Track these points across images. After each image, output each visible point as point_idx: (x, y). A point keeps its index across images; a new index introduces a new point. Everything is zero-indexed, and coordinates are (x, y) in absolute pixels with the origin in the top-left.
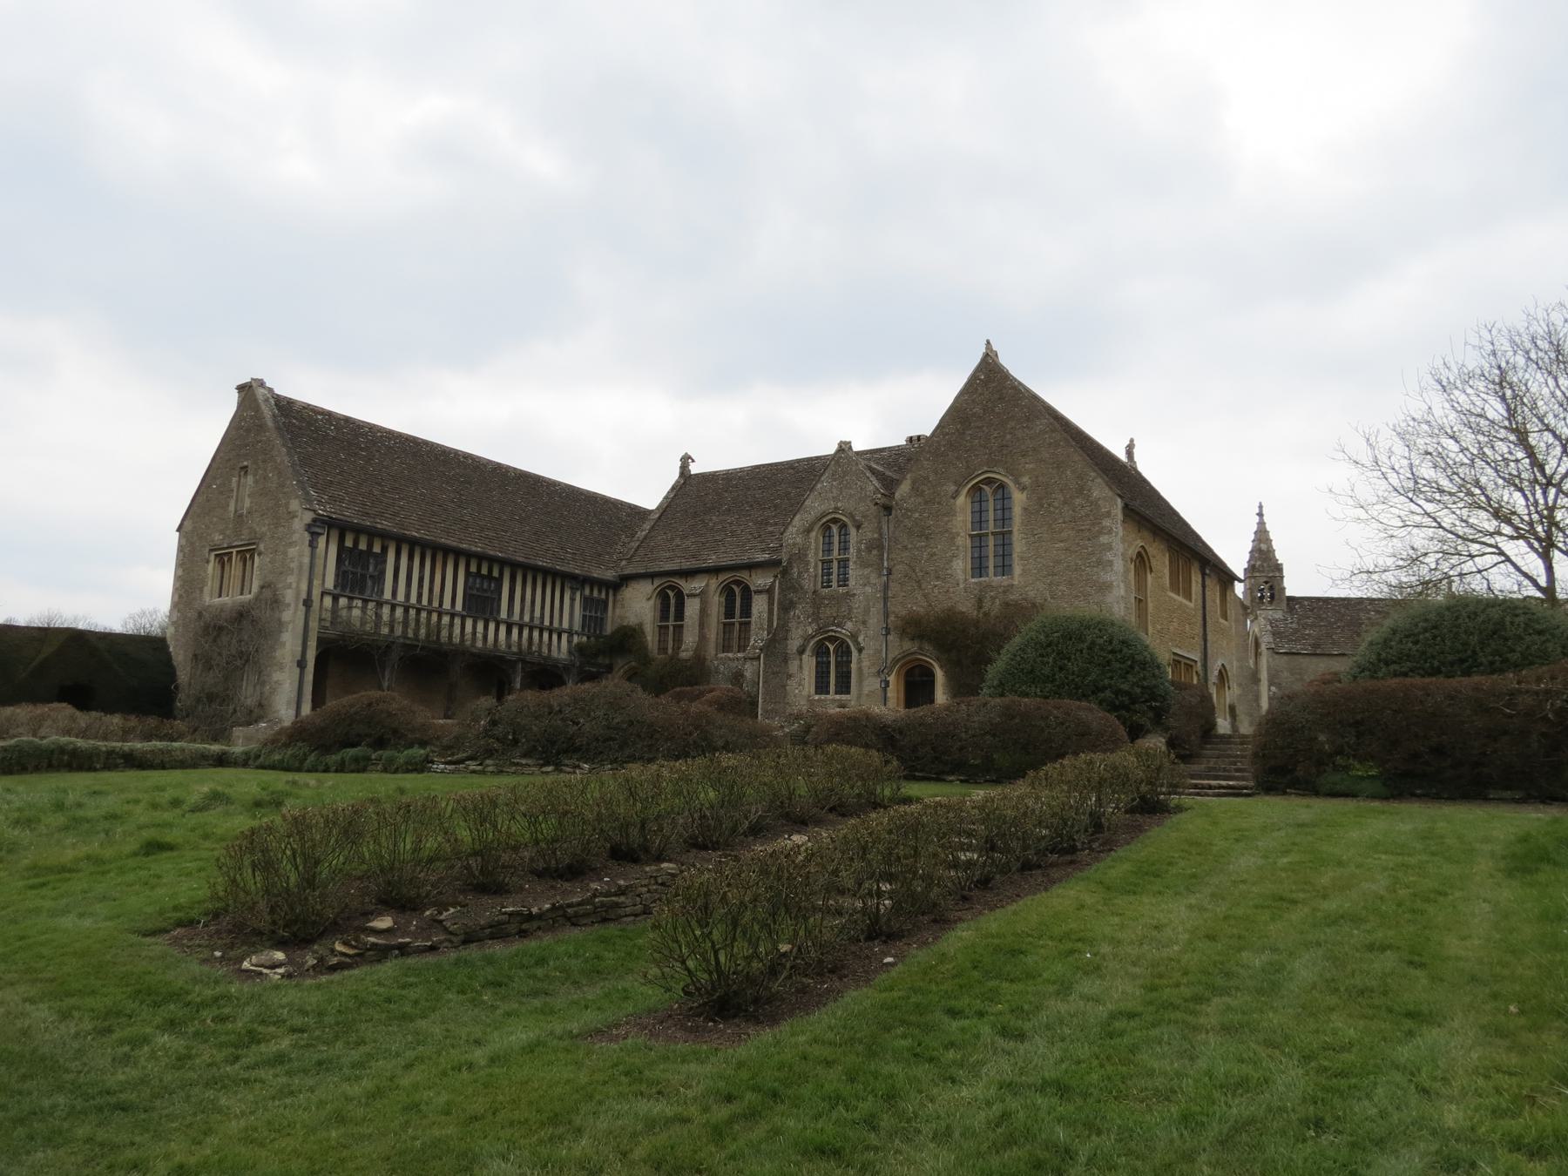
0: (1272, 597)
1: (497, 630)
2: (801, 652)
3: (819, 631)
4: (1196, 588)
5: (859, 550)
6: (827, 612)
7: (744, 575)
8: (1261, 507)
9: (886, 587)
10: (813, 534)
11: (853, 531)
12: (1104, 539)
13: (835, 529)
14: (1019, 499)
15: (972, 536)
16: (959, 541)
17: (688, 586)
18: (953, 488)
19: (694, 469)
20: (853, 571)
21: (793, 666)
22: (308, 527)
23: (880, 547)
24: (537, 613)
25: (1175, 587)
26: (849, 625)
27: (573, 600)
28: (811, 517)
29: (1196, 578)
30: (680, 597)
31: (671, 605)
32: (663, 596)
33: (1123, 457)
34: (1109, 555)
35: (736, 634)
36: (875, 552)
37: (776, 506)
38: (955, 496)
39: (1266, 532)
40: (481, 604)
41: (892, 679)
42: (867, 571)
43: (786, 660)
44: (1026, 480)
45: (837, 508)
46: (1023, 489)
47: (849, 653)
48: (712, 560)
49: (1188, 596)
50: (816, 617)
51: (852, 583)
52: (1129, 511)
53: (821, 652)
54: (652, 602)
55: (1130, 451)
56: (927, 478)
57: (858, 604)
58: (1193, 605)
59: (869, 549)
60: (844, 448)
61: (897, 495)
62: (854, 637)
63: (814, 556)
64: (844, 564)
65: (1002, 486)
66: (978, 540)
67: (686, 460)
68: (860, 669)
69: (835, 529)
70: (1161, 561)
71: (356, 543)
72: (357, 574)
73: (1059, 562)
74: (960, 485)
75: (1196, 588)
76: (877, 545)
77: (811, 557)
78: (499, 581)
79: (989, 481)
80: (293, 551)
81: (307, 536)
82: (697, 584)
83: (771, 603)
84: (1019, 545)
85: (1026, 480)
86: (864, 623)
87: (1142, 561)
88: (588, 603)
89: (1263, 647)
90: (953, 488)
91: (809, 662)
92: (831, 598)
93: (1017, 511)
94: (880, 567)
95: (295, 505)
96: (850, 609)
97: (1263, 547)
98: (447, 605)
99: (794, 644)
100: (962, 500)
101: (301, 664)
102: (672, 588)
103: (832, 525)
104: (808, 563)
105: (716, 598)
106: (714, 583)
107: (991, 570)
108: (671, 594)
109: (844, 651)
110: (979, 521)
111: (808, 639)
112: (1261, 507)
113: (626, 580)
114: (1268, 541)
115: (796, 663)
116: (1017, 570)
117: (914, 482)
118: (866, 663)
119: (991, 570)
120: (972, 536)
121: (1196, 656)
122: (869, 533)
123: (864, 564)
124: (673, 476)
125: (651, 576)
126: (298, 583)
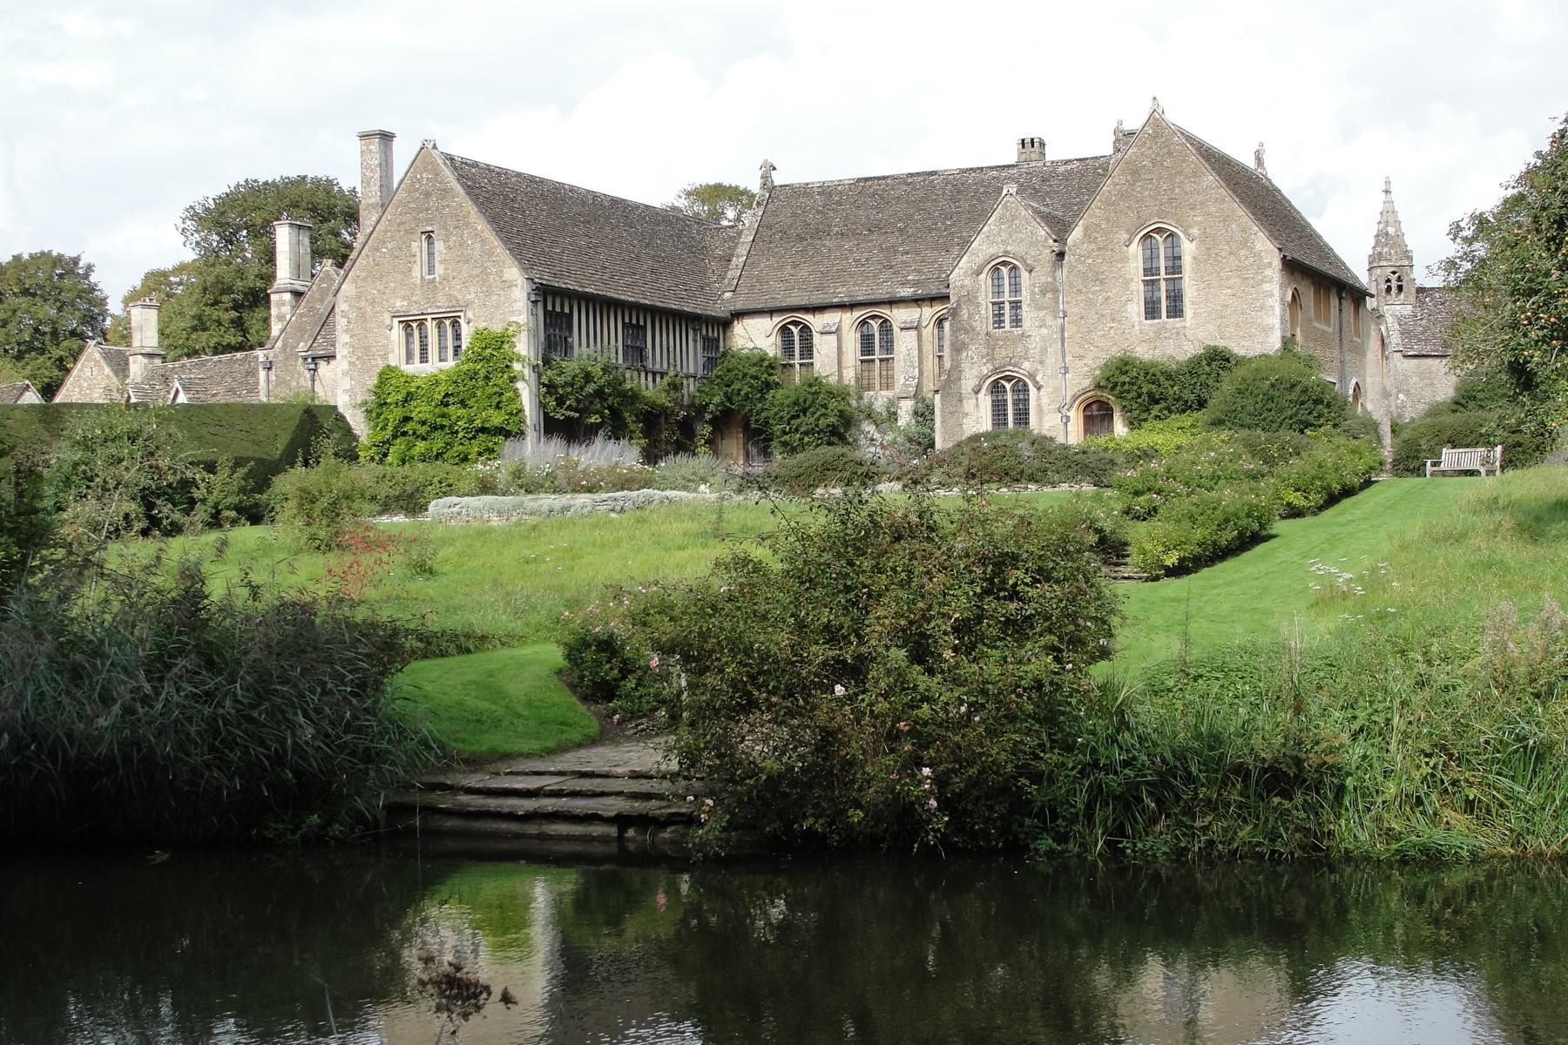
0: (1400, 288)
2: (977, 392)
3: (995, 371)
5: (1033, 293)
6: (1001, 354)
7: (885, 311)
8: (1388, 183)
10: (983, 276)
11: (1024, 275)
12: (1266, 287)
14: (1188, 249)
16: (1133, 286)
17: (816, 322)
18: (1126, 236)
19: (778, 179)
20: (1026, 313)
21: (968, 405)
23: (1055, 291)
25: (1318, 317)
26: (1026, 365)
27: (695, 341)
28: (980, 260)
29: (1334, 302)
31: (797, 340)
32: (784, 330)
33: (1251, 163)
36: (1049, 295)
37: (900, 230)
40: (636, 352)
42: (1042, 314)
44: (1195, 231)
47: (1026, 390)
48: (842, 296)
49: (1327, 322)
51: (1026, 324)
52: (1291, 267)
53: (996, 388)
55: (1259, 160)
56: (1099, 225)
57: (1034, 345)
59: (1043, 292)
62: (1032, 376)
63: (985, 298)
64: (1016, 306)
68: (1039, 406)
70: (1308, 295)
73: (1226, 306)
75: (1334, 311)
76: (1052, 289)
77: (981, 299)
79: (1159, 231)
85: (1195, 231)
88: (711, 344)
90: (1126, 236)
91: (986, 400)
93: (1187, 262)
94: (1055, 312)
96: (1027, 350)
97: (1391, 230)
99: (968, 384)
100: (1135, 248)
102: (795, 323)
105: (852, 334)
106: (848, 319)
108: (795, 330)
109: (1021, 388)
112: (1388, 183)
117: (1086, 229)
118: (1045, 401)
125: (771, 312)
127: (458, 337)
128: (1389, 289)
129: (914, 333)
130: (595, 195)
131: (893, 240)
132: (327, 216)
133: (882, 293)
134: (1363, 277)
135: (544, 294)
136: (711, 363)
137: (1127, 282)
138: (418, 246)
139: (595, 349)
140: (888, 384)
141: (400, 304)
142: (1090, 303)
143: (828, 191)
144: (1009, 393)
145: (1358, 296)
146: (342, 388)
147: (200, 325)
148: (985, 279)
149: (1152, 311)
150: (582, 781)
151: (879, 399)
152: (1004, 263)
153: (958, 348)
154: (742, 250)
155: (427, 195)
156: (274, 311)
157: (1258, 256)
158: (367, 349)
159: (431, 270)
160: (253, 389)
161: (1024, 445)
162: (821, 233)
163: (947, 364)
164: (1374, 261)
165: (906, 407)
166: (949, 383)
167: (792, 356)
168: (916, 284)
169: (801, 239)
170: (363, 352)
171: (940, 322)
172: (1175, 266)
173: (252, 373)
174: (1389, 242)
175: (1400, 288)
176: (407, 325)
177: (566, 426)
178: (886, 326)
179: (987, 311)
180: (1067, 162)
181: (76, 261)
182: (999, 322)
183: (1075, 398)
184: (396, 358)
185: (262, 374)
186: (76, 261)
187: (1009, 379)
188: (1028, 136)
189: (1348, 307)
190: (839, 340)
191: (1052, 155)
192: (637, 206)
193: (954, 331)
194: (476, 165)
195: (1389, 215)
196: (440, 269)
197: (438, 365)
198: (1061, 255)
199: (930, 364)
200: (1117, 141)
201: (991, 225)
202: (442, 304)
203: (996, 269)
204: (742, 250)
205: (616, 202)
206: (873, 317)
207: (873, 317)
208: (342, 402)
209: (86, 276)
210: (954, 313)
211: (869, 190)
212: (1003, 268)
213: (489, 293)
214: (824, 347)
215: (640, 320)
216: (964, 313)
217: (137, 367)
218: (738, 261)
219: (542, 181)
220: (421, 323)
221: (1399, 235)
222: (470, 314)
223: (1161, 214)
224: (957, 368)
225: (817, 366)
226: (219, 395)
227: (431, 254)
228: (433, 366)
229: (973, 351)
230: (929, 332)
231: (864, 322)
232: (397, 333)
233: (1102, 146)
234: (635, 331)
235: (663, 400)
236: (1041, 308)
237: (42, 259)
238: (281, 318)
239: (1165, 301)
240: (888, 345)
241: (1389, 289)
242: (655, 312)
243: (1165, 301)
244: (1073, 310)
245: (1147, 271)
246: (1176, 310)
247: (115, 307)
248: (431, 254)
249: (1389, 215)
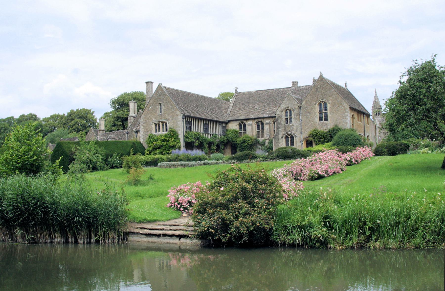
0: (379, 114)
2: (282, 138)
4: (362, 119)
7: (262, 120)
9: (301, 124)
11: (292, 112)
12: (346, 114)
13: (288, 111)
14: (329, 106)
17: (247, 123)
18: (315, 103)
19: (239, 91)
21: (280, 141)
25: (358, 120)
26: (293, 132)
28: (283, 108)
29: (362, 117)
32: (240, 125)
33: (344, 86)
34: (347, 117)
39: (377, 97)
40: (206, 131)
41: (303, 143)
44: (330, 101)
46: (329, 104)
47: (293, 137)
48: (253, 117)
49: (361, 122)
50: (285, 131)
51: (293, 123)
52: (352, 109)
53: (287, 137)
55: (346, 85)
57: (295, 127)
58: (362, 123)
59: (297, 116)
61: (302, 104)
62: (294, 134)
63: (284, 117)
64: (291, 119)
67: (236, 89)
68: (296, 141)
69: (288, 111)
70: (356, 116)
73: (337, 118)
74: (316, 102)
75: (362, 119)
76: (299, 115)
79: (322, 102)
80: (179, 123)
82: (250, 122)
83: (270, 126)
84: (329, 115)
85: (330, 101)
87: (353, 117)
88: (224, 128)
89: (377, 127)
90: (315, 103)
91: (284, 140)
92: (288, 126)
93: (328, 108)
94: (299, 120)
95: (178, 113)
97: (377, 101)
99: (280, 136)
100: (317, 106)
102: (242, 123)
109: (292, 137)
113: (230, 121)
114: (378, 99)
117: (306, 101)
118: (297, 140)
121: (363, 134)
125: (237, 120)
127: (166, 126)
128: (376, 114)
129: (268, 125)
130: (198, 95)
131: (264, 104)
132: (140, 100)
133: (261, 116)
134: (370, 111)
135: (185, 117)
136: (223, 132)
137: (315, 113)
138: (158, 107)
139: (198, 129)
140: (263, 136)
141: (154, 119)
142: (307, 118)
143: (250, 94)
144: (290, 138)
145: (368, 115)
146: (142, 138)
147: (114, 125)
148: (284, 113)
149: (321, 119)
150: (189, 227)
151: (261, 139)
152: (288, 109)
153: (278, 128)
154: (231, 107)
155: (160, 95)
156: (129, 121)
157: (344, 107)
158: (147, 129)
159: (161, 112)
160: (124, 138)
161: (260, 148)
162: (248, 103)
163: (276, 132)
164: (373, 107)
165: (267, 141)
166: (276, 136)
167: (242, 130)
168: (269, 114)
169: (243, 104)
170: (146, 130)
171: (274, 123)
172: (326, 109)
173: (124, 135)
174: (376, 104)
175: (379, 114)
176: (156, 125)
177: (189, 146)
178: (262, 124)
179: (284, 120)
180: (302, 86)
181: (90, 111)
182: (287, 122)
183: (304, 139)
184: (154, 132)
185: (126, 135)
186: (90, 111)
187: (289, 135)
188: (294, 81)
189: (366, 118)
190: (252, 126)
191: (299, 85)
192: (207, 97)
193: (277, 125)
194: (171, 89)
195: (376, 97)
196: (163, 112)
197: (163, 133)
198: (300, 107)
199: (272, 131)
200: (313, 82)
201: (285, 101)
202: (163, 120)
203: (286, 110)
204: (231, 107)
205: (202, 97)
206: (260, 121)
207: (260, 121)
208: (142, 141)
209: (92, 114)
210: (277, 120)
211: (259, 93)
212: (288, 110)
213: (173, 117)
214: (248, 128)
215: (207, 122)
216: (279, 121)
217: (100, 133)
218: (230, 109)
219: (186, 92)
220: (159, 125)
221: (378, 102)
222: (169, 122)
223: (323, 98)
224: (278, 132)
225: (247, 133)
226: (117, 139)
227: (161, 109)
228: (161, 133)
229: (281, 129)
230: (272, 125)
231: (257, 123)
232: (154, 126)
233: (311, 83)
234: (206, 125)
235: (212, 140)
236: (296, 119)
237: (83, 110)
238: (130, 122)
239: (324, 117)
240: (263, 128)
241: (376, 114)
242: (211, 121)
243: (324, 117)
244: (303, 119)
245: (320, 111)
246: (326, 119)
247: (98, 121)
248: (161, 109)
249: (376, 97)
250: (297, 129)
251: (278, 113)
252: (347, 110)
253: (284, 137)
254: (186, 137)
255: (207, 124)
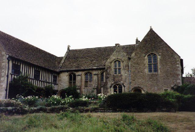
1: (39, 82)
2: (111, 87)
3: (115, 83)
5: (123, 67)
10: (112, 63)
15: (148, 64)
17: (77, 74)
18: (144, 55)
19: (71, 49)
21: (109, 90)
22: (7, 59)
24: (46, 79)
27: (52, 76)
30: (75, 76)
32: (70, 76)
35: (72, 83)
36: (127, 67)
38: (145, 56)
40: (37, 77)
43: (107, 89)
45: (118, 59)
46: (159, 55)
47: (122, 87)
48: (82, 68)
50: (114, 80)
54: (68, 76)
57: (123, 77)
59: (126, 67)
60: (138, 90)
62: (123, 84)
64: (119, 69)
65: (155, 54)
66: (150, 66)
69: (117, 63)
71: (15, 62)
72: (16, 70)
78: (40, 72)
79: (152, 54)
80: (3, 64)
81: (7, 61)
82: (80, 73)
84: (159, 66)
86: (125, 81)
90: (144, 55)
91: (112, 89)
95: (3, 53)
96: (122, 79)
98: (31, 77)
99: (109, 85)
100: (146, 57)
101: (6, 90)
102: (73, 74)
103: (117, 61)
104: (111, 69)
105: (84, 76)
107: (153, 71)
110: (150, 61)
111: (112, 84)
115: (110, 89)
116: (159, 71)
119: (153, 71)
120: (148, 64)
122: (125, 63)
123: (124, 69)
124: (66, 50)
126: (5, 71)
133: (90, 68)
149: (150, 71)
153: (107, 78)
168: (98, 66)
179: (113, 70)
187: (118, 85)
188: (117, 43)
203: (115, 62)
207: (88, 73)
233: (134, 43)
246: (156, 70)
250: (126, 79)
251: (107, 63)
252: (178, 62)
253: (112, 87)
254: (178, 116)
255: (38, 71)
